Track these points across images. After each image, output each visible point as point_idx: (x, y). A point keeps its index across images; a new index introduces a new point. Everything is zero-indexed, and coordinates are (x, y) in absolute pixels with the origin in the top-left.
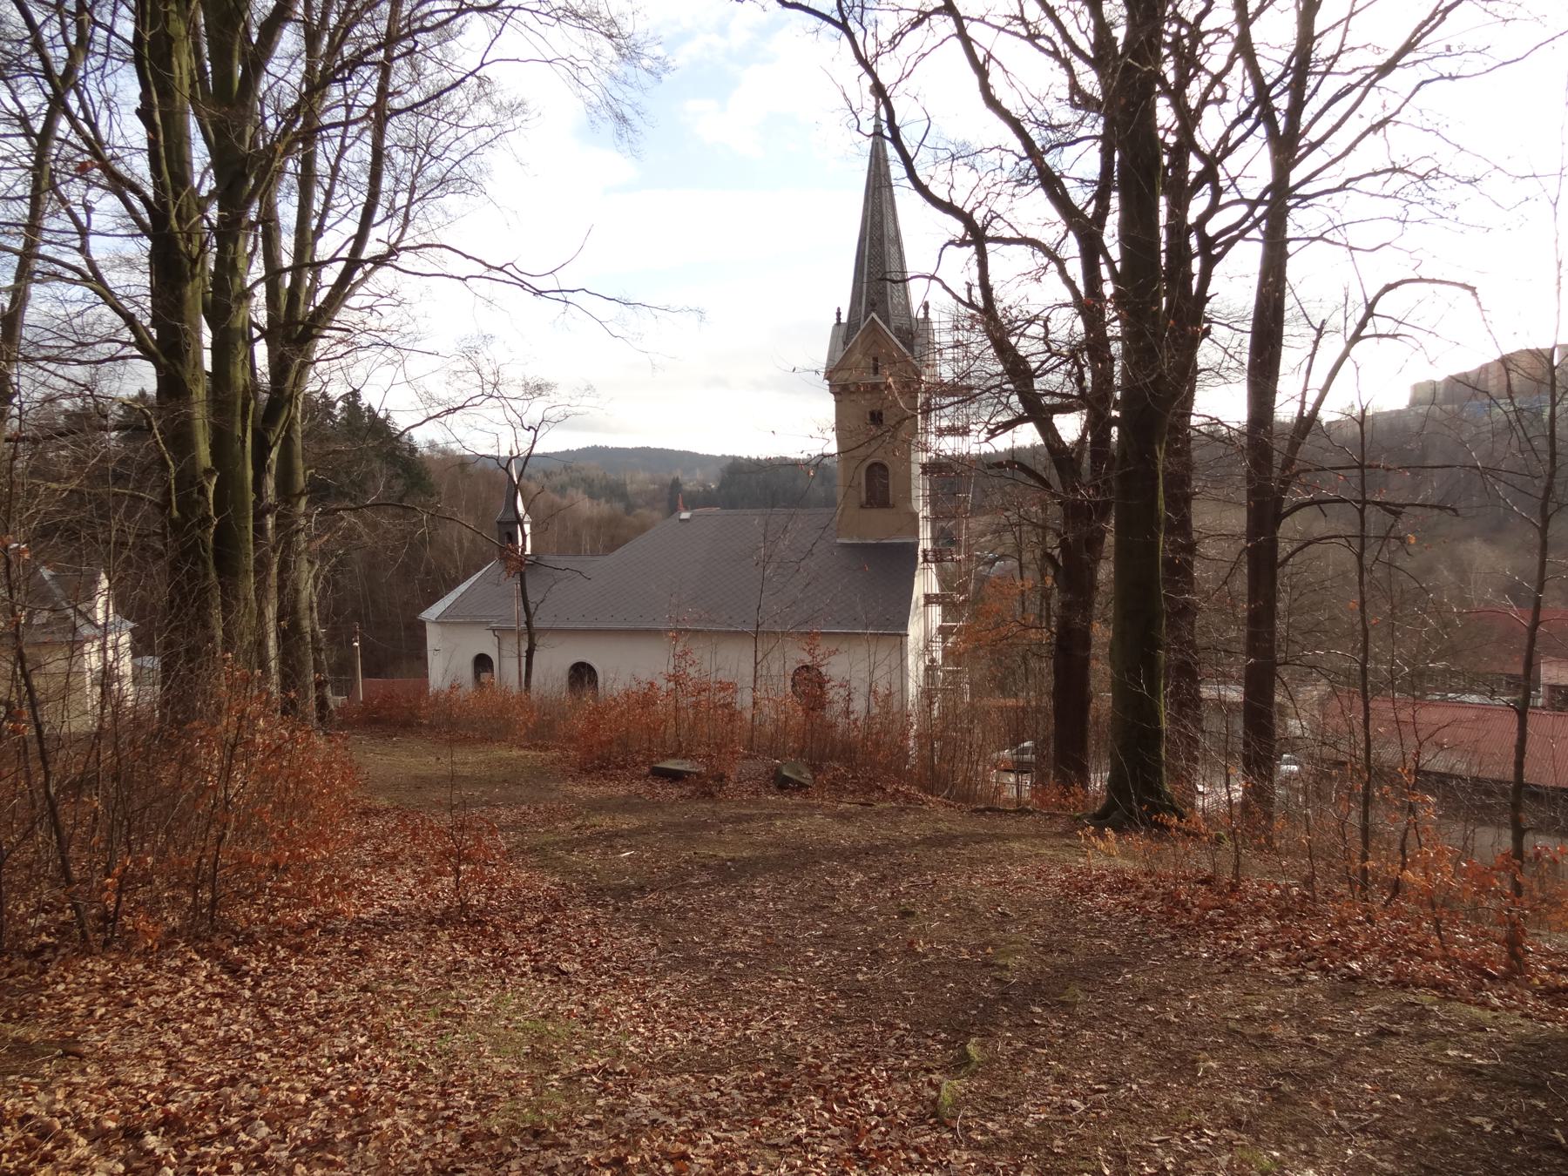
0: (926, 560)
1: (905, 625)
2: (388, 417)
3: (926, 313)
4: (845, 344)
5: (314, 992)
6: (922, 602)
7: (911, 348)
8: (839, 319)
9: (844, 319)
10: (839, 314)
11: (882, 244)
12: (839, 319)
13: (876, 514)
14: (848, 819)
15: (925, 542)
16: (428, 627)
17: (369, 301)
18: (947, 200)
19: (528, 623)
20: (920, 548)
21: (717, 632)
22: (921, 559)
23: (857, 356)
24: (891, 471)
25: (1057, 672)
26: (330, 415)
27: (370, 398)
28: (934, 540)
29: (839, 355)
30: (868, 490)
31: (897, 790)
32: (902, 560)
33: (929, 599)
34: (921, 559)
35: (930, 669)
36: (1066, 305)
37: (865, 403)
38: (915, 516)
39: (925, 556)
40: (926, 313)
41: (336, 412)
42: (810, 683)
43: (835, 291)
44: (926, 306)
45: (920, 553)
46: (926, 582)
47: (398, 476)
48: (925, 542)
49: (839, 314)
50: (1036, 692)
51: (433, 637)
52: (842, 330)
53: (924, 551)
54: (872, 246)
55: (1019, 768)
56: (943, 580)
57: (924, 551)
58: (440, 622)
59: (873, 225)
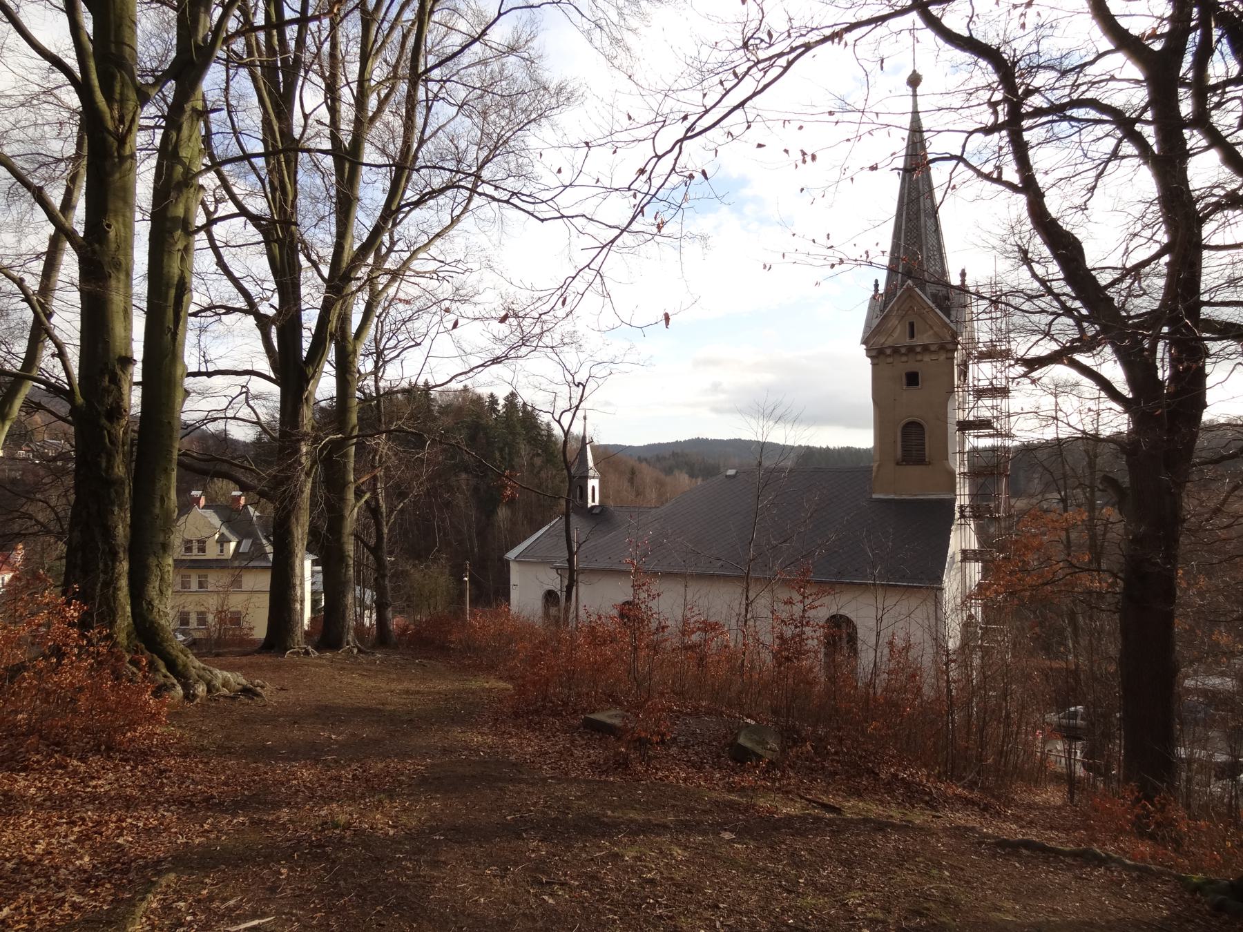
0: (962, 516)
1: (939, 579)
3: (963, 281)
4: (882, 311)
6: (959, 557)
9: (882, 289)
10: (876, 285)
11: (918, 218)
13: (914, 471)
15: (963, 496)
16: (512, 565)
17: (433, 266)
18: (965, 33)
19: (570, 561)
20: (957, 504)
21: (724, 576)
22: (957, 515)
23: (894, 321)
25: (1125, 632)
26: (495, 410)
27: (527, 396)
28: (973, 496)
29: (876, 322)
30: (903, 447)
31: (895, 776)
32: (939, 516)
33: (966, 556)
34: (957, 515)
35: (968, 625)
37: (903, 366)
38: (952, 474)
39: (962, 512)
40: (963, 281)
41: (500, 408)
42: (841, 632)
44: (963, 274)
45: (957, 509)
46: (963, 538)
47: (538, 455)
48: (963, 496)
49: (876, 285)
50: (1099, 647)
51: (516, 575)
53: (961, 506)
54: (909, 220)
55: (1070, 734)
56: (981, 533)
57: (961, 506)
58: (519, 560)
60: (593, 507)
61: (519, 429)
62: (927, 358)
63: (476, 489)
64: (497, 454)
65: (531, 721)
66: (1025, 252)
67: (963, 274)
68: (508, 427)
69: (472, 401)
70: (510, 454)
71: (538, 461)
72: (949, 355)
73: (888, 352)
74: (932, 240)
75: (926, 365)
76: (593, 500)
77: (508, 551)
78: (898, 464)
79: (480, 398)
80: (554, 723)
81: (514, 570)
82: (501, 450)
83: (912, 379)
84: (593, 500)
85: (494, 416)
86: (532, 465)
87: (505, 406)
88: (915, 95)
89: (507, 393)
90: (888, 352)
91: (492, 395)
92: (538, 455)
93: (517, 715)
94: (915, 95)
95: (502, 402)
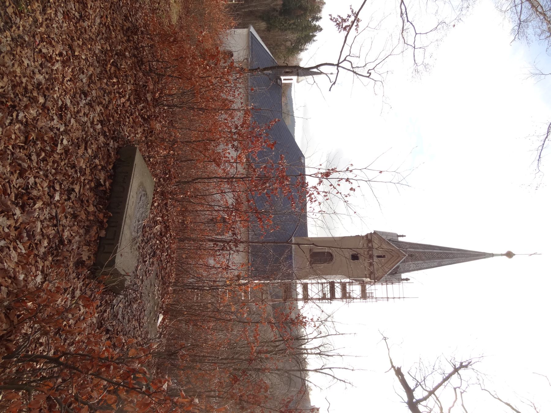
2: (314, 41)
3: (404, 280)
4: (390, 240)
5: (135, 296)
7: (392, 274)
8: (400, 236)
9: (400, 239)
10: (403, 236)
11: (438, 258)
12: (400, 236)
14: (396, 273)
23: (385, 246)
24: (332, 263)
26: (313, 20)
27: (319, 36)
29: (384, 237)
30: (319, 253)
36: (458, 374)
40: (404, 280)
41: (314, 22)
43: (413, 235)
47: (292, 44)
49: (403, 236)
52: (395, 238)
54: (438, 253)
58: (250, 34)
59: (447, 254)
60: (281, 79)
61: (305, 33)
62: (366, 264)
63: (274, 10)
64: (292, 22)
65: (121, 54)
66: (466, 366)
67: (407, 279)
68: (306, 27)
69: (319, 7)
70: (292, 28)
71: (288, 44)
72: (368, 276)
73: (370, 245)
74: (426, 265)
75: (363, 262)
76: (285, 80)
77: (254, 28)
78: (310, 250)
79: (320, 11)
80: (122, 95)
81: (245, 31)
82: (294, 24)
83: (355, 257)
84: (285, 80)
85: (310, 19)
86: (286, 41)
87: (315, 25)
88: (502, 255)
89: (322, 26)
90: (370, 245)
91: (321, 18)
92: (292, 44)
93: (131, 32)
94: (502, 255)
95: (317, 23)
